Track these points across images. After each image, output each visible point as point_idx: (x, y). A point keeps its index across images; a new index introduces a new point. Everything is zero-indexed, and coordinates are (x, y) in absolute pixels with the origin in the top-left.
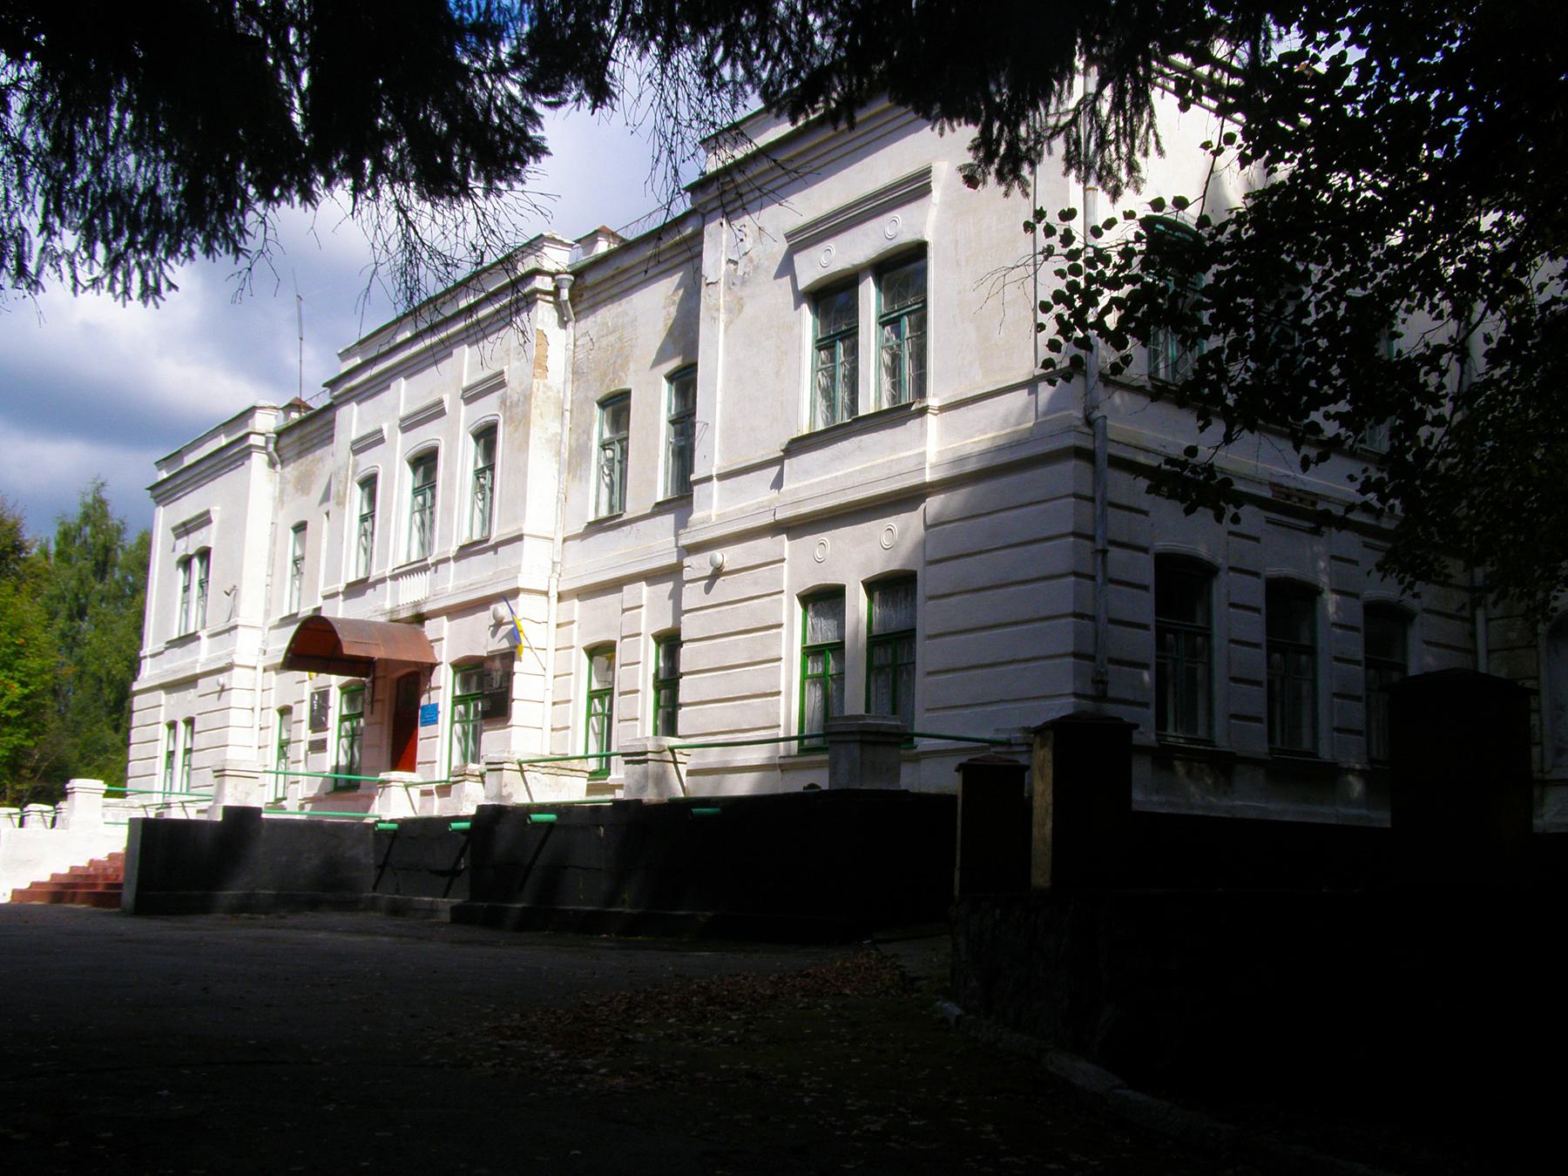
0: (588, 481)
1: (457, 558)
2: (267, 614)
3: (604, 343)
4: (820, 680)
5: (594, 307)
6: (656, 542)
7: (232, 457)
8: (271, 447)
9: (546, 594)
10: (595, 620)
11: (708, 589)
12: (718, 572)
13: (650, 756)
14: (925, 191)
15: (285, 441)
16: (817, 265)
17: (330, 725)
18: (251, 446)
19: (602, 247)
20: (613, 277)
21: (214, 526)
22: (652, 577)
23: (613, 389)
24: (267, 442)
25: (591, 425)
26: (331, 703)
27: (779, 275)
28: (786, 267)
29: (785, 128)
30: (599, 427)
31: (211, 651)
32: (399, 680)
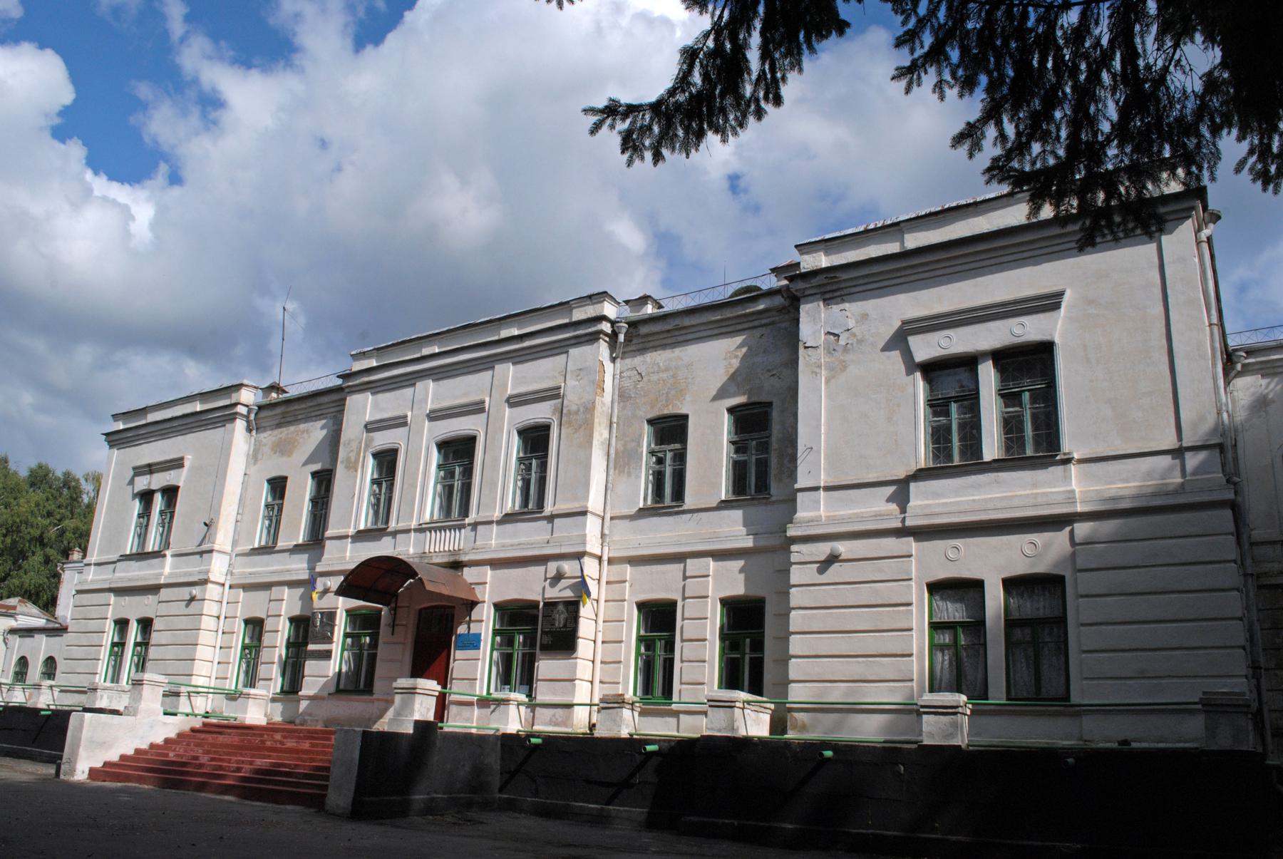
0: (638, 477)
1: (499, 522)
2: (235, 543)
3: (654, 377)
4: (139, 656)
5: (642, 351)
6: (298, 567)
7: (226, 416)
8: (252, 416)
11: (187, 606)
12: (833, 559)
13: (960, 710)
14: (1056, 306)
15: (263, 414)
16: (142, 483)
17: (335, 639)
19: (649, 309)
20: (668, 331)
21: (185, 470)
23: (666, 412)
24: (249, 412)
25: (641, 436)
26: (337, 622)
27: (887, 348)
28: (131, 482)
29: (1017, 214)
30: (264, 494)
31: (173, 567)
32: (420, 610)
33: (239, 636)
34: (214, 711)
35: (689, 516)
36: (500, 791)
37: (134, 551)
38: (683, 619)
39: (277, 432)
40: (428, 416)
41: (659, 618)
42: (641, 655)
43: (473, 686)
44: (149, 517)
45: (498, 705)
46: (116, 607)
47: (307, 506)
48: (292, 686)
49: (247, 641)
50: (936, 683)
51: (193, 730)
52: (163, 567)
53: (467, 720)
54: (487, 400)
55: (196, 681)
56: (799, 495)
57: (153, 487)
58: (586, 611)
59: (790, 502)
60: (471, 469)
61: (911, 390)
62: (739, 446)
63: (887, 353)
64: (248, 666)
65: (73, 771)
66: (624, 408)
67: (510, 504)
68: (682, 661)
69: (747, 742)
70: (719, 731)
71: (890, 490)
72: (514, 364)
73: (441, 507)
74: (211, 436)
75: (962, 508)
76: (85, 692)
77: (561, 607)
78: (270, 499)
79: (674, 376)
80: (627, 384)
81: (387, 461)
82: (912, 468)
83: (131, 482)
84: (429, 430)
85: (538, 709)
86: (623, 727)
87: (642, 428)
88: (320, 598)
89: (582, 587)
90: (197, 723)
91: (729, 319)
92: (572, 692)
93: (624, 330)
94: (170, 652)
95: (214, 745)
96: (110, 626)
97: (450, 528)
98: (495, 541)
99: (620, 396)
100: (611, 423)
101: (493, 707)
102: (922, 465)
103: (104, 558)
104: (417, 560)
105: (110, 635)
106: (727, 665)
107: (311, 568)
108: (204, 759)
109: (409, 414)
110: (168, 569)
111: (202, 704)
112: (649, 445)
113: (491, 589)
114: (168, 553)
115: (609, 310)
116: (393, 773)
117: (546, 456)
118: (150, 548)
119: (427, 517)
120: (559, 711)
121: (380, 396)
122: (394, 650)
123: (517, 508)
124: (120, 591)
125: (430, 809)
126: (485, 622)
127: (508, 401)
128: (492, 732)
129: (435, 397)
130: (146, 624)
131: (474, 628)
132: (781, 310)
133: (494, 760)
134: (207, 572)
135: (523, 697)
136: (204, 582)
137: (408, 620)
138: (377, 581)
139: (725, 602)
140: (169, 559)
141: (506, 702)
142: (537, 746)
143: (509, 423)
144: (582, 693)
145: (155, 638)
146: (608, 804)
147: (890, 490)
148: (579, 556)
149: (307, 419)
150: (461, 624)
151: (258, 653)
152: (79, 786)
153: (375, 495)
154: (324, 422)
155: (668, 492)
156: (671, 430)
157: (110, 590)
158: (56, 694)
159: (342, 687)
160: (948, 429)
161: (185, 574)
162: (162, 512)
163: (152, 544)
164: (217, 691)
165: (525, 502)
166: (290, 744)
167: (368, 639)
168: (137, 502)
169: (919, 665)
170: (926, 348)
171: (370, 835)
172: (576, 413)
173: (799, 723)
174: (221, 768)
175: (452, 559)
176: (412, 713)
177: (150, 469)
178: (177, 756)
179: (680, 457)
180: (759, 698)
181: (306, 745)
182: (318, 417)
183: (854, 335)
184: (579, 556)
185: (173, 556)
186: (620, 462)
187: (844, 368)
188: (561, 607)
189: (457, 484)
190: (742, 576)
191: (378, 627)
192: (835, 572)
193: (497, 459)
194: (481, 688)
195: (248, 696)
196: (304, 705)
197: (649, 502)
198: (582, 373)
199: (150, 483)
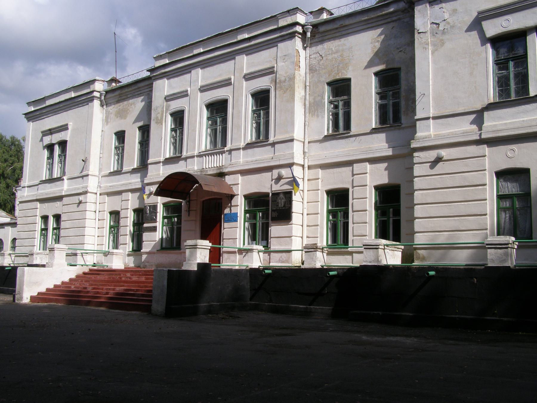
0: (323, 117)
1: (244, 149)
2: (100, 170)
3: (330, 57)
4: (56, 235)
5: (322, 41)
6: (135, 181)
7: (88, 99)
8: (103, 98)
9: (96, 194)
10: (115, 204)
11: (78, 206)
12: (439, 160)
13: (510, 246)
15: (109, 96)
16: (47, 140)
17: (158, 220)
18: (94, 97)
19: (325, 16)
20: (337, 29)
21: (69, 131)
22: (133, 191)
23: (338, 77)
24: (101, 95)
25: (323, 93)
26: (158, 211)
27: (470, 29)
28: (42, 140)
31: (69, 186)
32: (204, 201)
33: (107, 222)
34: (98, 263)
35: (354, 138)
36: (251, 299)
37: (47, 178)
38: (353, 199)
39: (117, 105)
40: (199, 89)
41: (339, 199)
42: (330, 221)
43: (235, 243)
44: (53, 158)
45: (247, 253)
46: (41, 209)
47: (137, 146)
48: (137, 248)
49: (112, 224)
50: (502, 230)
51: (84, 273)
52: (63, 186)
53: (233, 261)
54: (232, 77)
55: (86, 247)
56: (418, 123)
57: (54, 142)
58: (296, 198)
59: (413, 127)
60: (226, 119)
61: (484, 55)
62: (382, 95)
63: (469, 33)
64: (114, 237)
65: (21, 298)
66: (313, 77)
67: (249, 138)
68: (353, 223)
69: (387, 268)
70: (370, 262)
71: (473, 117)
72: (246, 55)
73: (211, 142)
74: (82, 110)
75: (516, 126)
76: (27, 256)
77: (282, 196)
78: (117, 144)
79: (342, 56)
80: (314, 62)
81: (178, 117)
82: (486, 103)
83: (42, 140)
84: (201, 97)
85: (272, 254)
86: (317, 262)
87: (324, 88)
88: (148, 197)
89: (294, 182)
90: (86, 270)
91: (372, 18)
92: (291, 243)
93: (310, 30)
94: (70, 232)
95: (95, 281)
96: (39, 220)
97: (216, 154)
98: (242, 159)
99: (310, 70)
100: (305, 86)
101: (244, 254)
102: (492, 101)
103: (32, 183)
104: (199, 173)
105: (39, 225)
106: (380, 224)
107: (142, 181)
108: (90, 289)
109: (189, 89)
110: (65, 187)
111: (91, 260)
112: (329, 97)
113: (242, 187)
114: (65, 178)
115: (301, 18)
116: (186, 292)
117: (268, 108)
118: (55, 176)
119: (203, 148)
120: (284, 254)
121: (172, 80)
122: (190, 223)
123: (254, 140)
124: (42, 201)
125: (210, 311)
126: (239, 206)
127: (244, 77)
128: (244, 268)
129: (203, 79)
130: (57, 218)
131: (234, 210)
132: (404, 11)
133: (246, 284)
134: (87, 187)
135: (261, 248)
136: (86, 193)
137: (197, 207)
138: (177, 186)
139: (377, 188)
140: (66, 181)
141: (251, 250)
142: (269, 274)
143: (246, 90)
144: (297, 244)
145: (63, 225)
146: (310, 305)
147: (473, 117)
148: (290, 165)
149: (133, 97)
150: (226, 208)
151: (118, 230)
152: (25, 306)
153: (173, 137)
154: (142, 97)
155: (342, 125)
156: (341, 88)
157: (37, 200)
158: (13, 258)
159: (164, 245)
160: (507, 78)
161: (75, 189)
162: (59, 156)
163: (56, 174)
164: (99, 252)
165: (258, 136)
166: (135, 278)
167: (176, 219)
168: (46, 151)
169: (491, 219)
170: (493, 28)
171: (174, 326)
172: (285, 81)
173: (421, 256)
174: (98, 293)
175: (218, 171)
176: (196, 259)
177: (51, 132)
178: (75, 287)
179: (347, 104)
180: (398, 243)
181: (143, 279)
182: (139, 95)
183: (448, 23)
184: (290, 165)
185: (68, 179)
186: (312, 109)
187: (442, 43)
188: (282, 196)
189: (219, 128)
190: (387, 172)
191: (181, 212)
192: (440, 167)
193: (240, 112)
194: (240, 244)
195: (112, 254)
196: (144, 257)
197: (330, 132)
198: (286, 57)
199: (51, 140)
